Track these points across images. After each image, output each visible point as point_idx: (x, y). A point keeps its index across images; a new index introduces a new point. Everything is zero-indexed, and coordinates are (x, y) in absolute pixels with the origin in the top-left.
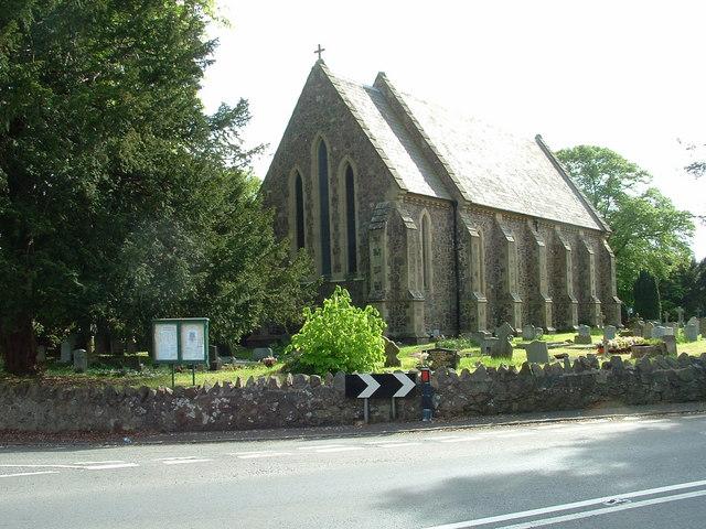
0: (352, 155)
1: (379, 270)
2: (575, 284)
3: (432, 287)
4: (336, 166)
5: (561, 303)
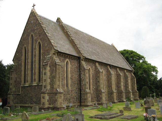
0: (41, 39)
1: (45, 80)
2: (124, 86)
3: (70, 87)
4: (36, 43)
5: (120, 93)
